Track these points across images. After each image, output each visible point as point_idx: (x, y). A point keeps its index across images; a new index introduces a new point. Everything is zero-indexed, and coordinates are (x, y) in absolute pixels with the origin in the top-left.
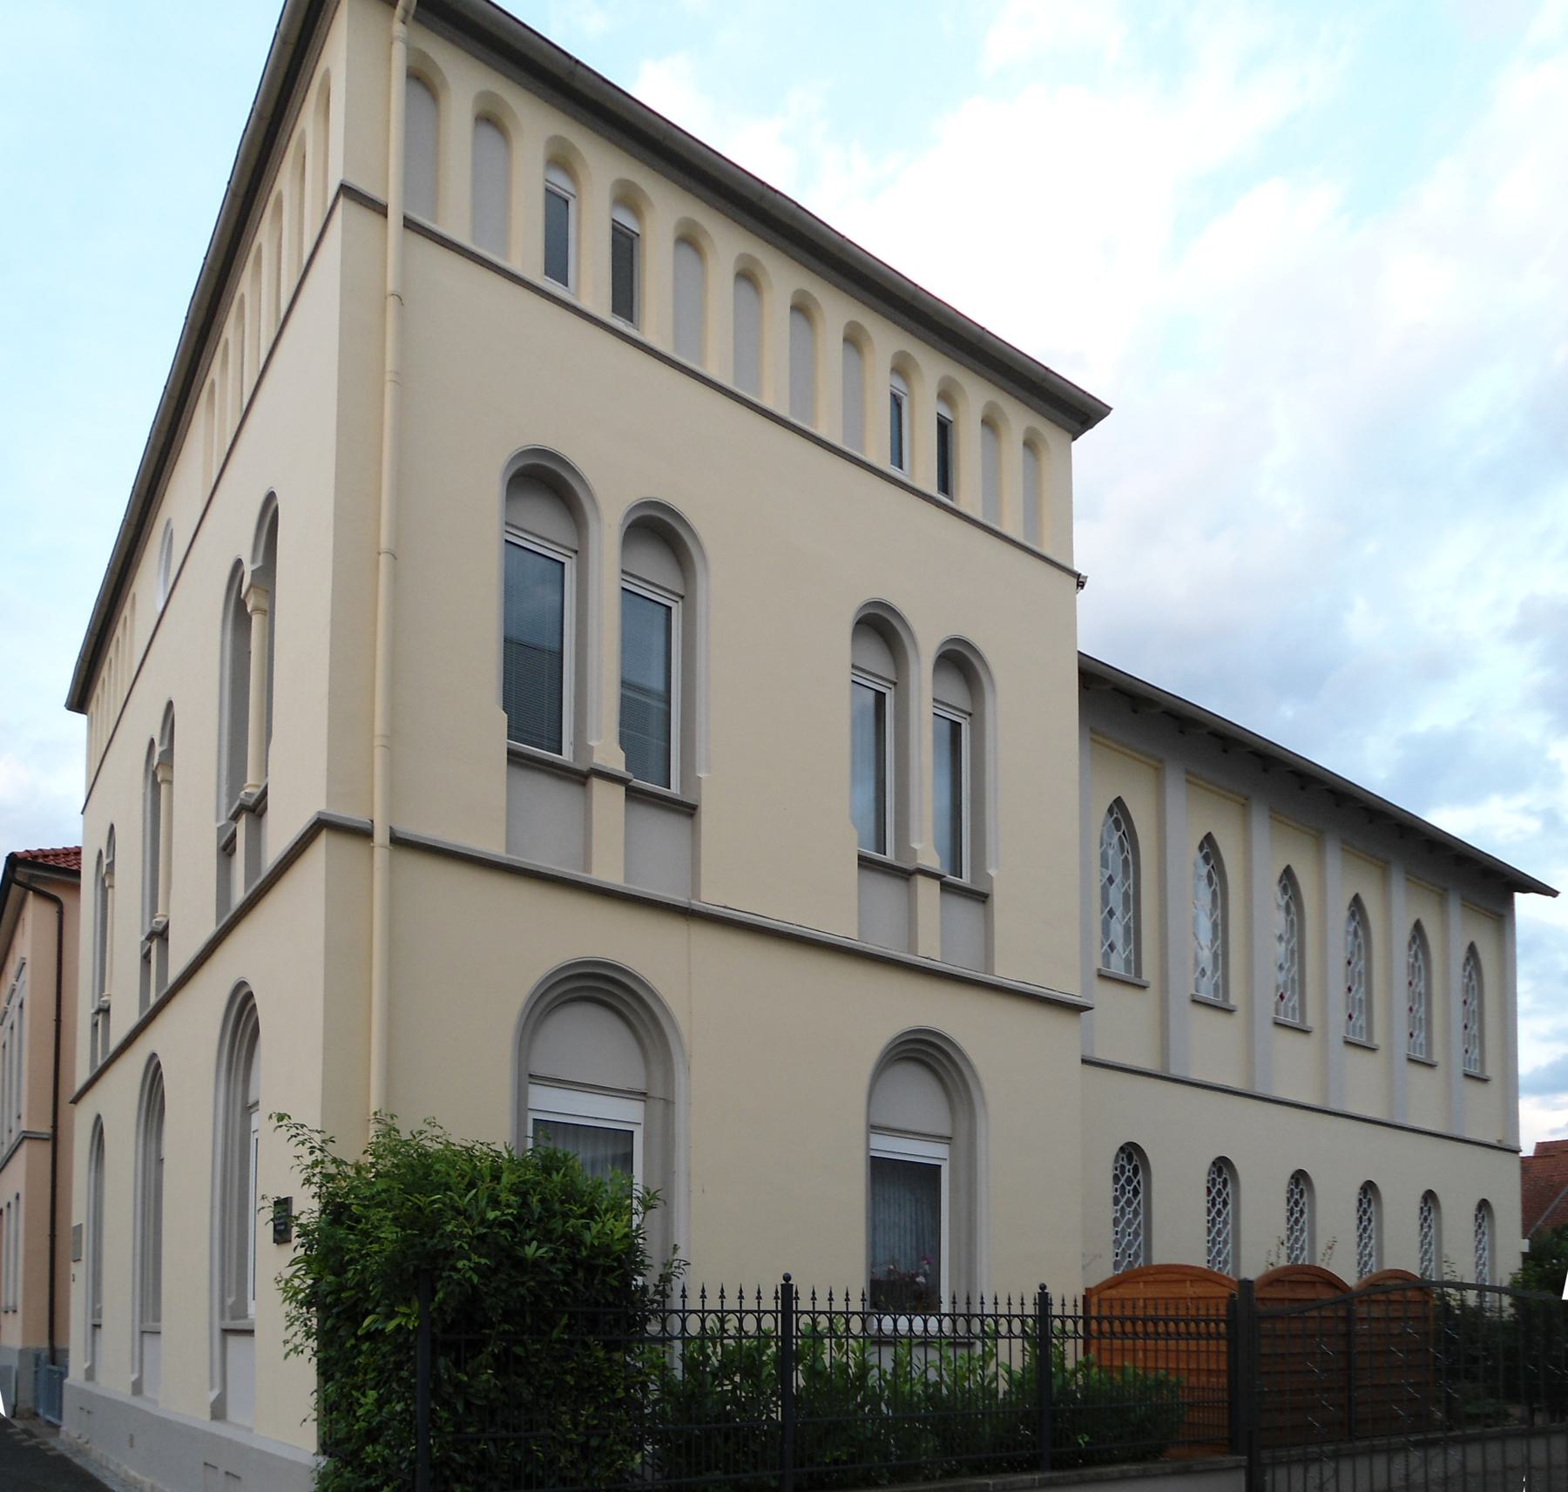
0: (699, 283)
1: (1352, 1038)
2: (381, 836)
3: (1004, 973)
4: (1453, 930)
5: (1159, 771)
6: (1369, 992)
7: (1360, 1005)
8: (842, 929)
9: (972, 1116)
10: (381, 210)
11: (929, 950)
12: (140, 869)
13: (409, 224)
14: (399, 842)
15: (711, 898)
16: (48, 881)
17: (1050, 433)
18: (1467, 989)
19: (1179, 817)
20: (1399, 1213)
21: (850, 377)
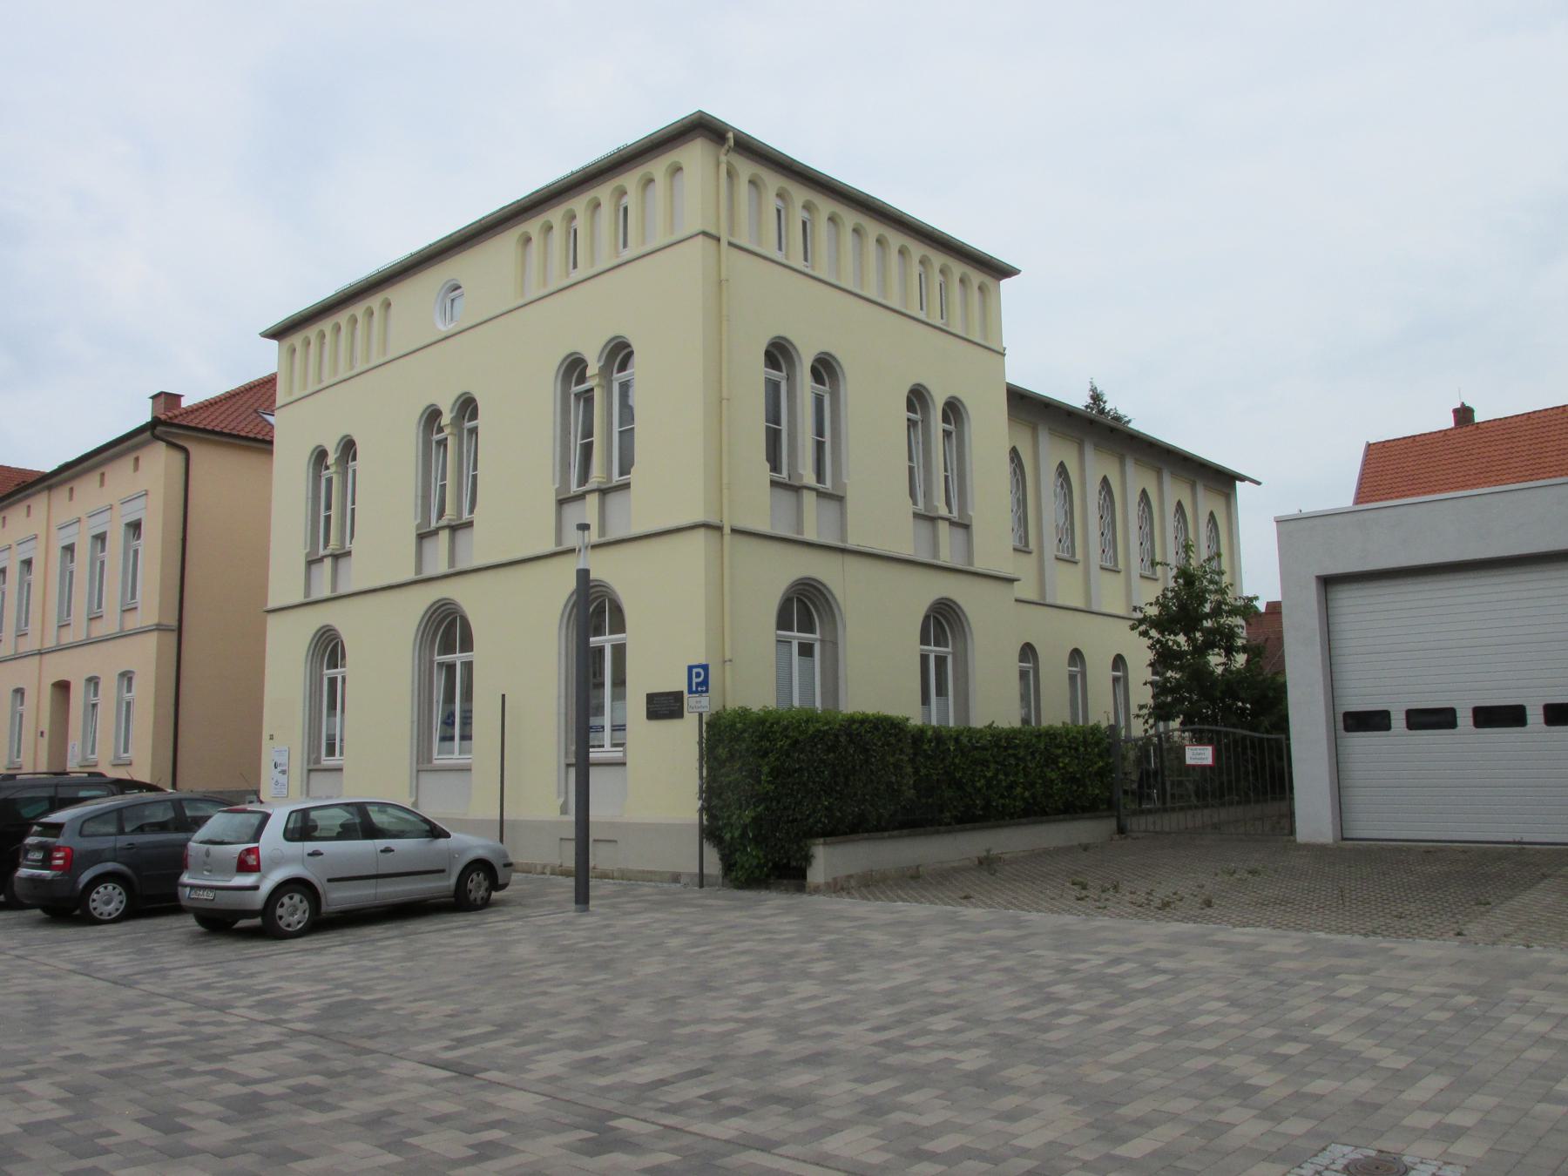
0: (843, 249)
1: (1060, 554)
2: (727, 530)
3: (978, 566)
4: (1207, 502)
5: (1034, 429)
6: (1153, 545)
7: (1067, 532)
8: (906, 551)
9: (835, 628)
10: (730, 244)
11: (945, 558)
12: (1375, 835)
13: (730, 244)
14: (734, 531)
15: (852, 542)
16: (178, 436)
17: (988, 280)
18: (1141, 518)
19: (1053, 451)
20: (1054, 671)
21: (899, 273)
